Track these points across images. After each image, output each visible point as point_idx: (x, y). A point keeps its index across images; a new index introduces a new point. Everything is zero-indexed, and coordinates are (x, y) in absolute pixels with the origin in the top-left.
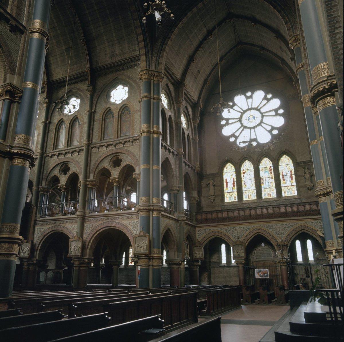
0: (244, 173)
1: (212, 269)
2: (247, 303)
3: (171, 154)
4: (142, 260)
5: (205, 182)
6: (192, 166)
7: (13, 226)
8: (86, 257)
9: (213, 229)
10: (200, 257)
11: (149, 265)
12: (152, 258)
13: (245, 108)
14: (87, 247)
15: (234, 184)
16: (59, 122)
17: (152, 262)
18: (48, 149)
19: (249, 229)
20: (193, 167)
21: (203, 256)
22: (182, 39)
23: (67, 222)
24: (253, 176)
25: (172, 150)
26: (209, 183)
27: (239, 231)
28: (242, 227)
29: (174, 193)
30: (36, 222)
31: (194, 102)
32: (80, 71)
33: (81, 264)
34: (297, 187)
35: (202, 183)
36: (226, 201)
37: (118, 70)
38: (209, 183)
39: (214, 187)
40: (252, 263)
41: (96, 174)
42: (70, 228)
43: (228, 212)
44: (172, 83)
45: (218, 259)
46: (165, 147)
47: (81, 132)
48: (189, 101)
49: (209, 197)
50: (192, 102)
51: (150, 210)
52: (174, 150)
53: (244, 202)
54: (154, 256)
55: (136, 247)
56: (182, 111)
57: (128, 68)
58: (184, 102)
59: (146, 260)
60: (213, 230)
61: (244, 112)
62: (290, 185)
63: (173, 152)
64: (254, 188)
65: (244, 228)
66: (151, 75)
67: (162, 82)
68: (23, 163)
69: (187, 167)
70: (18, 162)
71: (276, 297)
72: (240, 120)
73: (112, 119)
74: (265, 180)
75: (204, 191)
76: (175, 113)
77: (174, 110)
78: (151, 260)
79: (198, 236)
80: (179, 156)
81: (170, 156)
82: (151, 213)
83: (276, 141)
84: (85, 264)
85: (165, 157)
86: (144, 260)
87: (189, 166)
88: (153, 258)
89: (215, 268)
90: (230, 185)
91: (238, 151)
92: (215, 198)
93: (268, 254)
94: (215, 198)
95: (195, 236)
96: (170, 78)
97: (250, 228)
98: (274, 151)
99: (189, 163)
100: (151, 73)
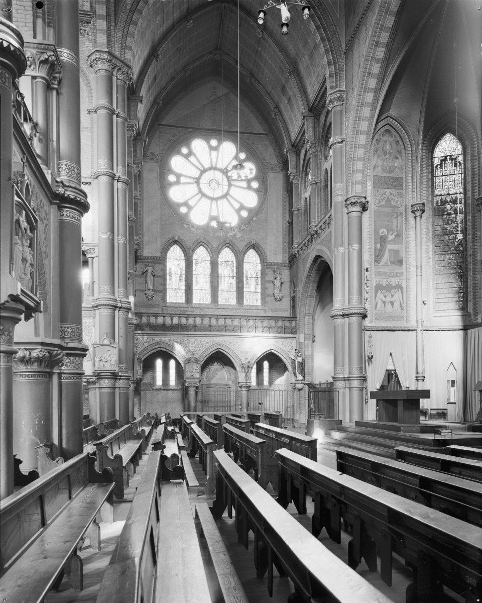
0: (196, 264)
7: (70, 329)
9: (157, 339)
13: (207, 165)
15: (181, 276)
19: (207, 343)
22: (154, 10)
24: (208, 270)
27: (194, 345)
34: (262, 295)
36: (168, 301)
38: (147, 271)
43: (164, 317)
53: (194, 306)
60: (159, 341)
62: (254, 290)
64: (208, 287)
66: (115, 68)
68: (70, 216)
70: (68, 215)
72: (197, 181)
74: (224, 278)
82: (116, 312)
83: (245, 228)
89: (147, 391)
90: (175, 278)
91: (193, 229)
98: (241, 241)
100: (116, 64)
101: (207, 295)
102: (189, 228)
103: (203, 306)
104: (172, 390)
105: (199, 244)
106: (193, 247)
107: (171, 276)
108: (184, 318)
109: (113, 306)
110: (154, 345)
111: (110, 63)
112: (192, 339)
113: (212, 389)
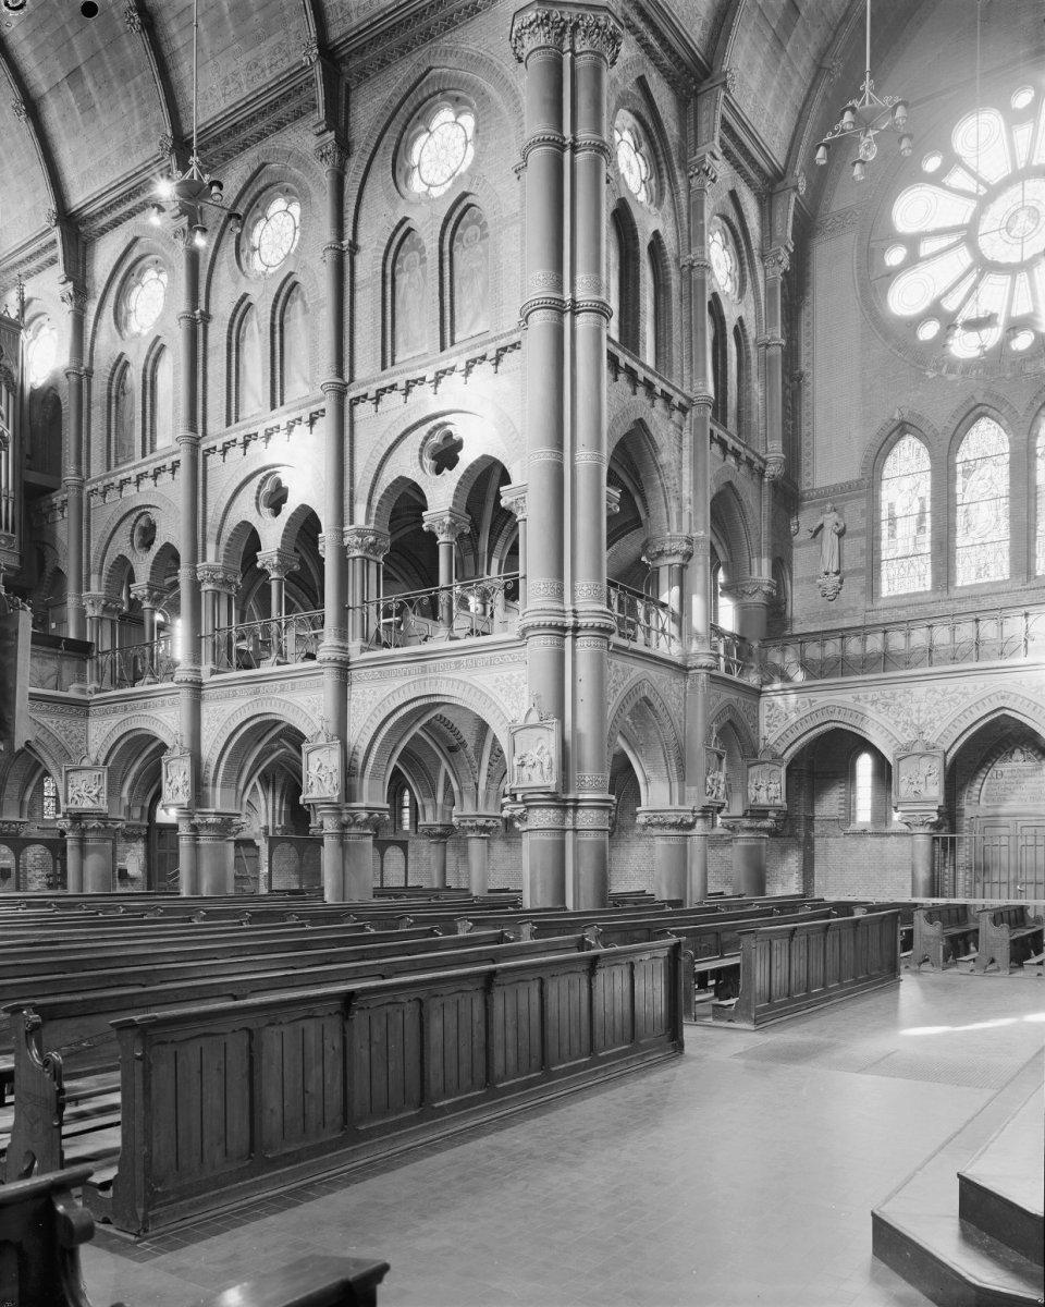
0: (967, 473)
1: (818, 843)
2: (925, 967)
3: (659, 403)
4: (537, 811)
5: (805, 521)
6: (752, 457)
8: (361, 800)
10: (769, 799)
11: (565, 830)
12: (571, 804)
13: (995, 170)
14: (360, 767)
15: (921, 520)
16: (236, 310)
17: (574, 818)
18: (210, 424)
20: (756, 460)
21: (784, 799)
23: (293, 684)
25: (664, 386)
26: (819, 523)
27: (923, 706)
28: (939, 688)
29: (670, 565)
30: (201, 690)
31: (769, 172)
32: (286, 65)
33: (344, 826)
35: (793, 528)
37: (428, 36)
38: (822, 526)
39: (839, 537)
40: (967, 822)
41: (375, 504)
42: (306, 704)
43: (843, 637)
44: (664, 72)
45: (843, 807)
46: (723, 443)
47: (314, 343)
48: (748, 169)
49: (818, 581)
50: (760, 171)
51: (565, 629)
52: (674, 388)
54: (581, 797)
55: (516, 767)
56: (716, 218)
57: (470, 15)
58: (722, 168)
59: (552, 813)
61: (994, 192)
63: (667, 398)
65: (945, 693)
67: (613, 63)
69: (731, 460)
71: (695, 974)
72: (968, 234)
73: (419, 271)
75: (801, 559)
76: (677, 222)
77: (675, 206)
78: (571, 811)
79: (768, 725)
80: (694, 413)
81: (655, 415)
82: (568, 641)
84: (359, 824)
85: (633, 417)
86: (544, 811)
87: (736, 454)
88: (576, 805)
90: (906, 528)
91: (952, 377)
92: (841, 582)
93: (1034, 788)
94: (841, 582)
95: (757, 725)
96: (659, 49)
97: (970, 691)
99: (740, 443)
100: (562, 20)
101: (1000, 558)
102: (941, 376)
103: (984, 590)
104: (895, 834)
105: (971, 415)
106: (953, 427)
107: (892, 519)
108: (899, 634)
109: (599, 629)
110: (967, 713)
111: (547, 25)
112: (919, 690)
113: (1003, 831)
